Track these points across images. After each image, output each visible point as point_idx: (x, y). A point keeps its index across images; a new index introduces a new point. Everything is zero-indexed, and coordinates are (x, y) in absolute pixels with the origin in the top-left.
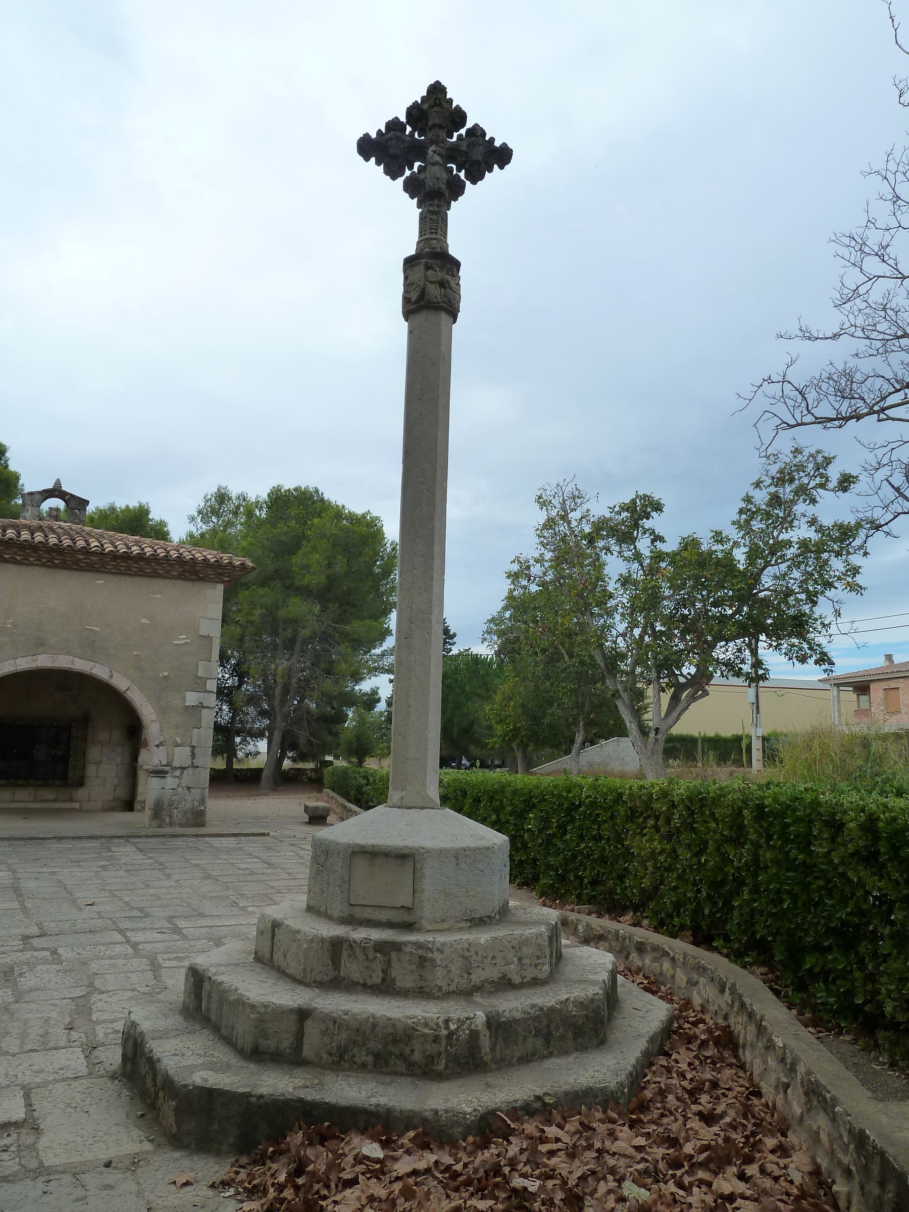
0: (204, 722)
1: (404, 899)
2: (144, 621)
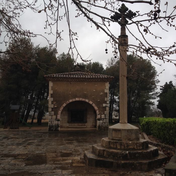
0: (107, 110)
1: (120, 136)
2: (94, 90)
